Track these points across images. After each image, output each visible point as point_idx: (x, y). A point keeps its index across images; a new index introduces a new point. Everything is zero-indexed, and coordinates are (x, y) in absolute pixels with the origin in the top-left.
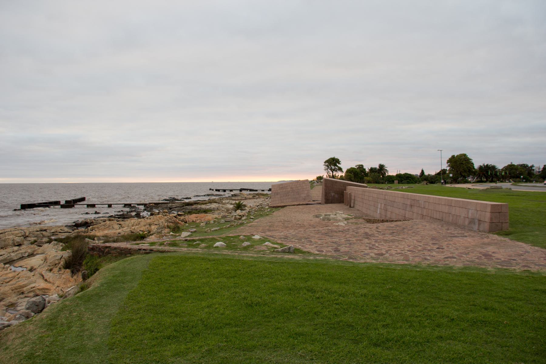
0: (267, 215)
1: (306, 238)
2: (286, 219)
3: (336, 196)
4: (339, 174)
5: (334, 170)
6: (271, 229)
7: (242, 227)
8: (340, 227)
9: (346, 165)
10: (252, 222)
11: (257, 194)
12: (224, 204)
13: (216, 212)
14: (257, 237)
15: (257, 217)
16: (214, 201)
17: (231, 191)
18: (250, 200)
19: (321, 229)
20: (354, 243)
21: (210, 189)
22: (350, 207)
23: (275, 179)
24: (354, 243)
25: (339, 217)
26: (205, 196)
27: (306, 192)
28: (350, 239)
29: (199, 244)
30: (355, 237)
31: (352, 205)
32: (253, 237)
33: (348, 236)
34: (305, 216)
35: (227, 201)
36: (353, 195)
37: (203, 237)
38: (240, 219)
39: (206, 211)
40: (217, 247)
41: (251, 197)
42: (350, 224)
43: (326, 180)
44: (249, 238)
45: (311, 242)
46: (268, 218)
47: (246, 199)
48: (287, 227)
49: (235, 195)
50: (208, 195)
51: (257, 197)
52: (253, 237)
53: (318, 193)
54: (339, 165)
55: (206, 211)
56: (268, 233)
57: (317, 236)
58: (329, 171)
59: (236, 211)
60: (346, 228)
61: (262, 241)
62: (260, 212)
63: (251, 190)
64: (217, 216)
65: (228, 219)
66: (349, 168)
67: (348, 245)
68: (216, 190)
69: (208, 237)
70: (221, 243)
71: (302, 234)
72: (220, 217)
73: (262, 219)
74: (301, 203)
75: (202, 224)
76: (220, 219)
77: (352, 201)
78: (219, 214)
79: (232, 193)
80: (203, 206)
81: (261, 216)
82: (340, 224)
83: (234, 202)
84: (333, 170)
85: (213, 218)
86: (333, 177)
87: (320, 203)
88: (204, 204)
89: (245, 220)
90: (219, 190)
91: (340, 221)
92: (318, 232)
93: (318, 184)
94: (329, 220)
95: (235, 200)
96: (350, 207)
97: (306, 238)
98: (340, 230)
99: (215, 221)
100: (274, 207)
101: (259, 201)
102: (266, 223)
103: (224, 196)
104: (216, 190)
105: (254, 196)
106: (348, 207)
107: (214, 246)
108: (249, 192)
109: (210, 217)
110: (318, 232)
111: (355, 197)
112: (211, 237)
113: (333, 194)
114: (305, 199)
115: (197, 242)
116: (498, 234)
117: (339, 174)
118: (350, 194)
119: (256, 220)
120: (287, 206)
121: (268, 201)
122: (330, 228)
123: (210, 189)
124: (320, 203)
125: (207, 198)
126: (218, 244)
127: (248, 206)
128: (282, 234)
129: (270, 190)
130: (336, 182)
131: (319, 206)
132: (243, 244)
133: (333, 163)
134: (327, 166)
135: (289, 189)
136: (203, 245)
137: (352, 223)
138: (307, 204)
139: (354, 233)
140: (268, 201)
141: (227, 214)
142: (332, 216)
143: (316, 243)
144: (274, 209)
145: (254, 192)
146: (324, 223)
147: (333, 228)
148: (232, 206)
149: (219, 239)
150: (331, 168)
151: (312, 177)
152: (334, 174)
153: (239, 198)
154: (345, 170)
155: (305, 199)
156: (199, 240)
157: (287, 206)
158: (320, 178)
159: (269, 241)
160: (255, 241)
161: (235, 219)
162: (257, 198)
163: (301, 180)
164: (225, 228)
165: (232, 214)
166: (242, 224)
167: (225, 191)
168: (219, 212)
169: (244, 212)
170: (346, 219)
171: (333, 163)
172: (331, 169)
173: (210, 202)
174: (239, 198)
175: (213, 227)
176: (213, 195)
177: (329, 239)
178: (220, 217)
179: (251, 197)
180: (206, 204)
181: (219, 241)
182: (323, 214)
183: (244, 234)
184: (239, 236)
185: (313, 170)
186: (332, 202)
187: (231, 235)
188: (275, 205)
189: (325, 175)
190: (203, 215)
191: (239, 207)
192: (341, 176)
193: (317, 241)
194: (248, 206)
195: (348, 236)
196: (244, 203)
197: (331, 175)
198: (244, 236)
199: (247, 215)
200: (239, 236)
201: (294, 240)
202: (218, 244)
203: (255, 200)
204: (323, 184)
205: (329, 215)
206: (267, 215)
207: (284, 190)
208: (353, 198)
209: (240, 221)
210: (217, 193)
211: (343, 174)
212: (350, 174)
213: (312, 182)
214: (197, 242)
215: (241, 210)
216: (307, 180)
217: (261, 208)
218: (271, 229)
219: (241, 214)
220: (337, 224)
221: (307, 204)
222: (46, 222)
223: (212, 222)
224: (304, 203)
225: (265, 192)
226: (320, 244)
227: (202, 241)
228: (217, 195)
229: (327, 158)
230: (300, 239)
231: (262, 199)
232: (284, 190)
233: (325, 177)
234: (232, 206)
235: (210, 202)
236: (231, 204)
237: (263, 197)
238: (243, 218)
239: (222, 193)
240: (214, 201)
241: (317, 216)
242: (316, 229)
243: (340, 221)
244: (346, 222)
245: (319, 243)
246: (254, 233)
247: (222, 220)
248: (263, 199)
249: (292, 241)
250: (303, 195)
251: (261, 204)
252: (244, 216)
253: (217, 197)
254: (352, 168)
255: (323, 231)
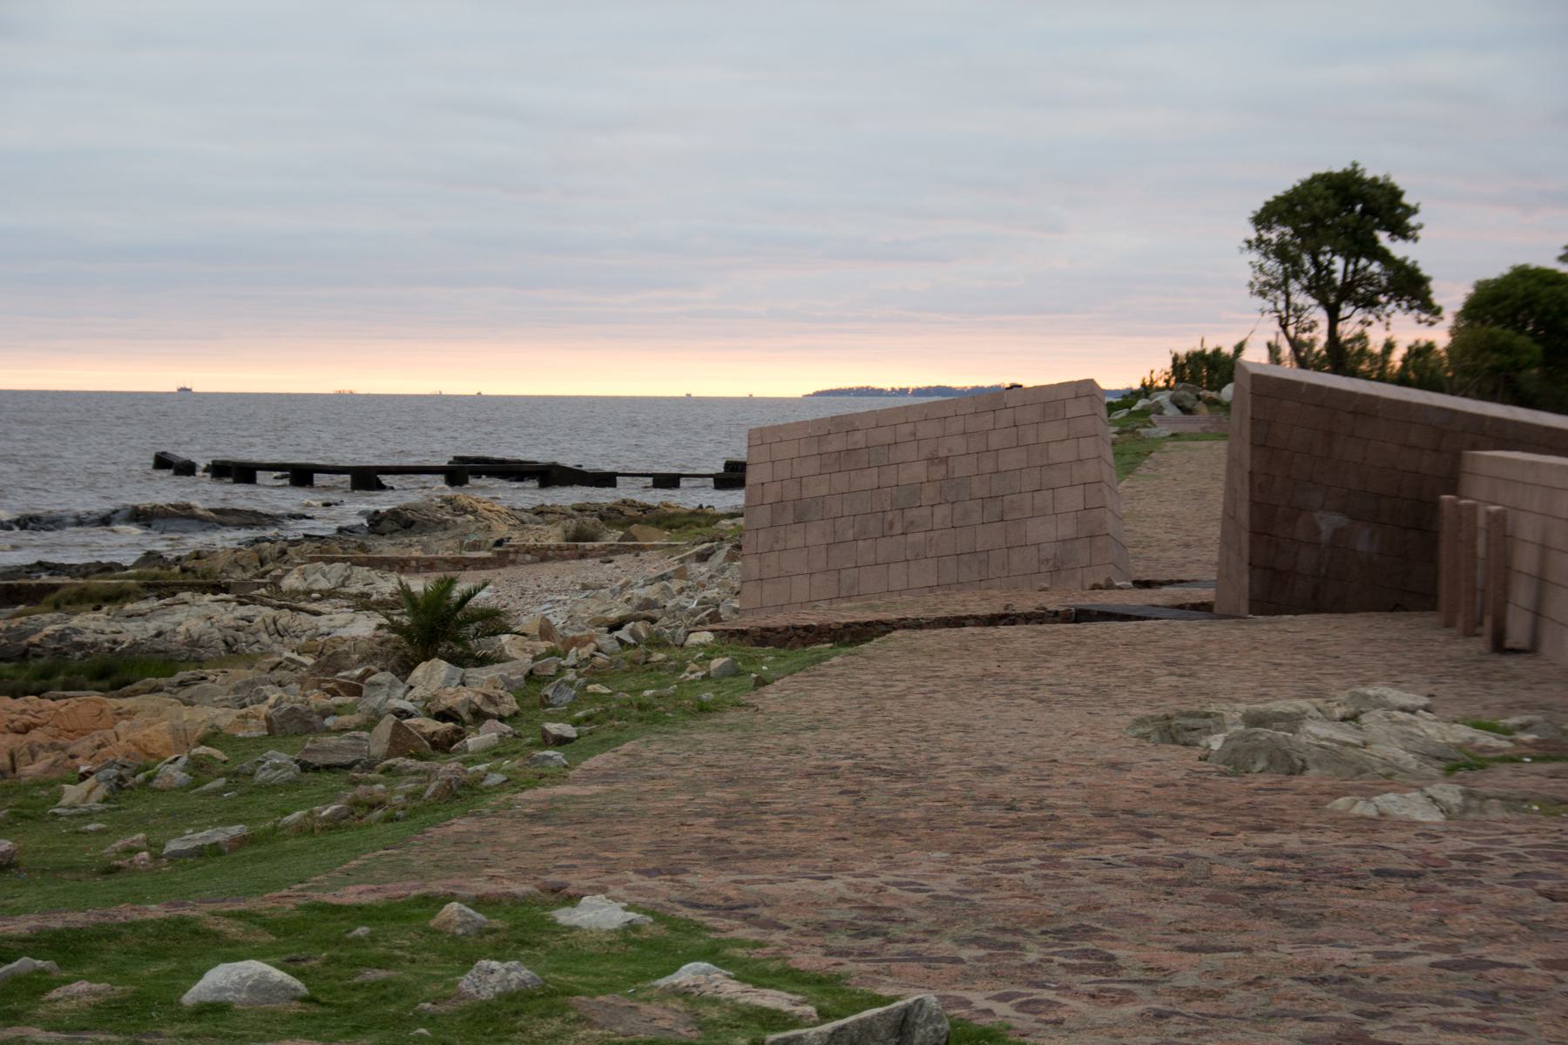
0: (703, 709)
1: (1063, 935)
2: (881, 752)
3: (1364, 542)
4: (1397, 331)
5: (1347, 292)
6: (739, 838)
7: (461, 825)
8: (1391, 838)
9: (1461, 248)
10: (561, 777)
11: (613, 516)
12: (292, 602)
13: (220, 681)
14: (599, 914)
15: (602, 726)
16: (201, 578)
17: (366, 479)
18: (546, 572)
19: (1201, 847)
20: (1528, 996)
21: (162, 462)
22: (1499, 645)
23: (787, 375)
24: (1528, 996)
25: (1384, 740)
26: (105, 521)
27: (1072, 499)
28: (1492, 952)
29: (36, 986)
30: (1537, 930)
31: (1517, 632)
32: (564, 916)
33: (1466, 921)
34: (1053, 723)
35: (324, 577)
36: (1527, 528)
37: (78, 919)
38: (443, 745)
39: (114, 671)
40: (215, 1010)
41: (552, 536)
42: (1496, 813)
43: (1265, 388)
44: (521, 925)
45: (1108, 965)
46: (708, 735)
47: (504, 555)
48: (884, 828)
49: (401, 522)
50: (141, 517)
51: (613, 537)
52: (564, 916)
53: (1185, 507)
54: (1399, 249)
55: (114, 671)
56: (707, 880)
57: (1166, 912)
58: (1301, 299)
59: (404, 668)
60: (1453, 844)
61: (646, 951)
62: (635, 681)
63: (550, 475)
64: (225, 718)
65: (331, 747)
66: (1496, 268)
67: (1465, 1011)
68: (221, 470)
69: (125, 913)
70: (254, 968)
71: (1027, 893)
72: (256, 730)
73: (650, 747)
74: (1026, 605)
75: (72, 793)
76: (257, 744)
77: (1522, 594)
78: (244, 696)
79: (382, 502)
80: (92, 624)
81: (648, 715)
82: (1390, 802)
83: (386, 585)
84: (1333, 297)
85: (181, 738)
86: (1340, 357)
87: (1203, 608)
88: (98, 600)
89: (494, 753)
90: (244, 473)
91: (1392, 777)
92: (1178, 878)
93: (1189, 425)
94: (1292, 766)
95: (401, 565)
96: (1499, 645)
97: (1063, 935)
98: (1395, 862)
99: (199, 767)
100: (765, 637)
101: (634, 577)
102: (695, 786)
103: (297, 530)
104: (221, 470)
105: (580, 535)
106: (1480, 645)
107: (189, 998)
108: (527, 495)
109: (152, 721)
110: (1178, 878)
111: (1544, 548)
112: (156, 912)
113: (1328, 523)
114: (1058, 569)
115: (23, 964)
116: (514, 897)
117: (1397, 331)
118: (1501, 530)
119: (598, 761)
120: (886, 627)
121: (714, 582)
122: (1293, 842)
123: (162, 462)
124: (1203, 608)
125: (126, 546)
126: (222, 979)
127: (528, 623)
128: (839, 884)
129: (732, 476)
130: (1365, 407)
131: (1193, 632)
132: (466, 983)
133: (1336, 226)
134: (1281, 252)
135: (919, 471)
136: (81, 990)
137: (1512, 802)
138: (1082, 616)
139: (1528, 899)
140: (714, 582)
141: (317, 699)
142: (1318, 730)
143: (1155, 975)
144: (767, 660)
145: (562, 483)
146: (1233, 789)
147: (1329, 838)
148: (364, 627)
149: (234, 930)
150: (1323, 271)
151: (1130, 363)
152: (1347, 330)
153: (443, 547)
154: (1451, 295)
155: (1058, 569)
156: (35, 944)
157: (886, 627)
158: (1204, 372)
159: (712, 954)
160: (578, 951)
161: (402, 742)
162: (607, 555)
163: (1028, 382)
164: (302, 830)
165: (373, 699)
166: (462, 793)
167: (301, 476)
168: (241, 674)
169: (482, 677)
170: (1458, 763)
171: (1336, 226)
172: (1321, 287)
173: (162, 581)
174: (443, 547)
175: (181, 819)
176: (183, 515)
177: (1284, 950)
178: (256, 730)
179: (552, 536)
180: (117, 597)
181: (234, 952)
182: (1234, 714)
183: (481, 886)
184: (433, 902)
185: (1146, 294)
186: (1320, 598)
187: (350, 895)
188: (779, 620)
189: (1252, 333)
190: (84, 704)
191: (438, 629)
192: (1420, 353)
193: (1167, 959)
194: (528, 623)
195: (1466, 921)
196: (484, 599)
197: (1321, 337)
198: (479, 903)
199: (509, 705)
200: (433, 902)
201: (944, 946)
202: (222, 979)
203: (590, 570)
204: (1240, 421)
205: (1293, 721)
206: (703, 709)
207: (869, 479)
208: (1525, 559)
209: (447, 767)
210: (238, 496)
211: (1440, 336)
212: (1502, 333)
213: (1132, 406)
214: (23, 964)
215: (455, 660)
216: (1087, 389)
217: (643, 642)
218: (739, 838)
219: (455, 697)
220: (1363, 808)
221: (1082, 616)
222: (574, 883)
223: (173, 773)
224: (1053, 602)
225: (686, 499)
226: (1197, 994)
227: (69, 948)
228: (224, 518)
229: (1285, 180)
230: (1001, 942)
231: (656, 564)
232: (869, 479)
233: (1256, 356)
234: (364, 627)
235: (162, 581)
236: (363, 603)
237: (662, 538)
238: (473, 741)
239: (288, 499)
240: (201, 578)
241: (1172, 732)
242: (1161, 849)
243: (1392, 777)
244: (1451, 794)
245: (1188, 979)
246: (575, 881)
247: (277, 756)
248: (670, 565)
249: (931, 961)
250: (1043, 531)
251: (647, 611)
252: (479, 716)
253: (225, 540)
254: (1522, 274)
255: (1228, 871)
